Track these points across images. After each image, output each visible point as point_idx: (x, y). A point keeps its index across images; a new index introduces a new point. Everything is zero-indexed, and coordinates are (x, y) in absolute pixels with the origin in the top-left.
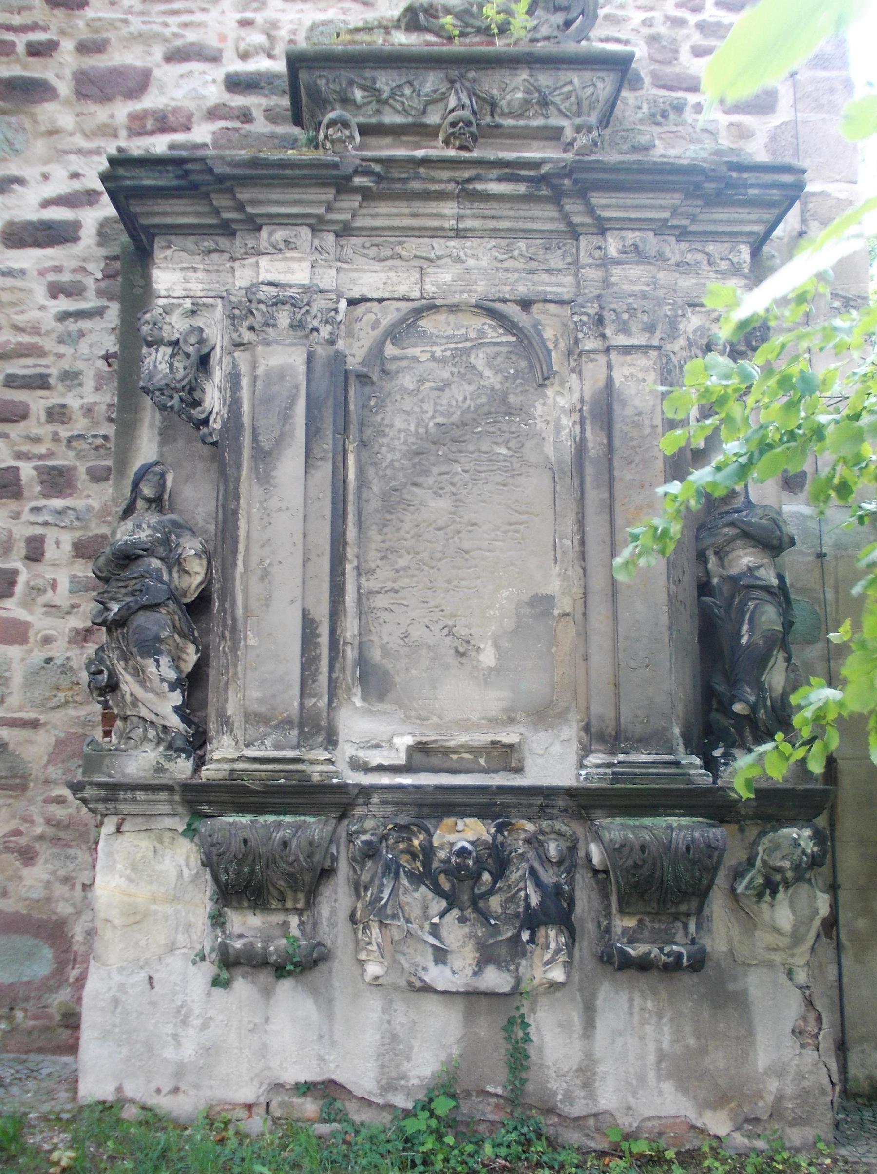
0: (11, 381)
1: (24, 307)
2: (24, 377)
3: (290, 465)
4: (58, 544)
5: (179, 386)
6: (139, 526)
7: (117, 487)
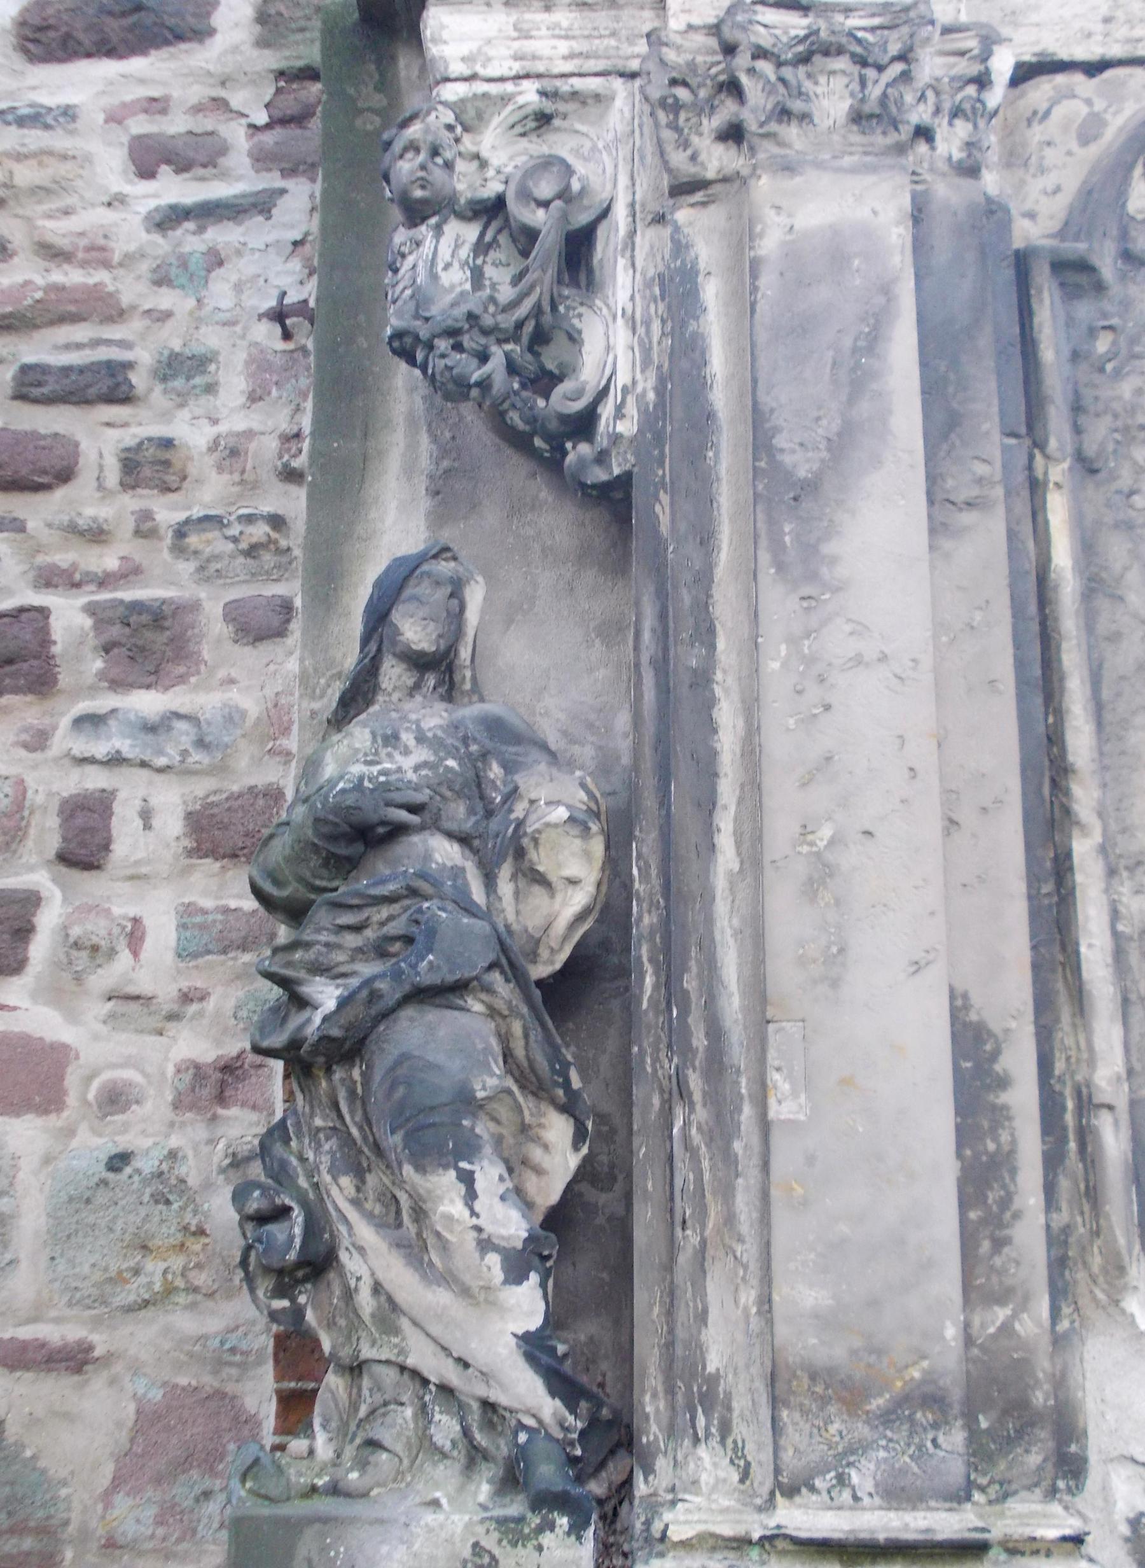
0: (32, 386)
1: (70, 200)
2: (66, 370)
3: (881, 524)
4: (146, 816)
5: (507, 321)
6: (392, 739)
7: (316, 641)
